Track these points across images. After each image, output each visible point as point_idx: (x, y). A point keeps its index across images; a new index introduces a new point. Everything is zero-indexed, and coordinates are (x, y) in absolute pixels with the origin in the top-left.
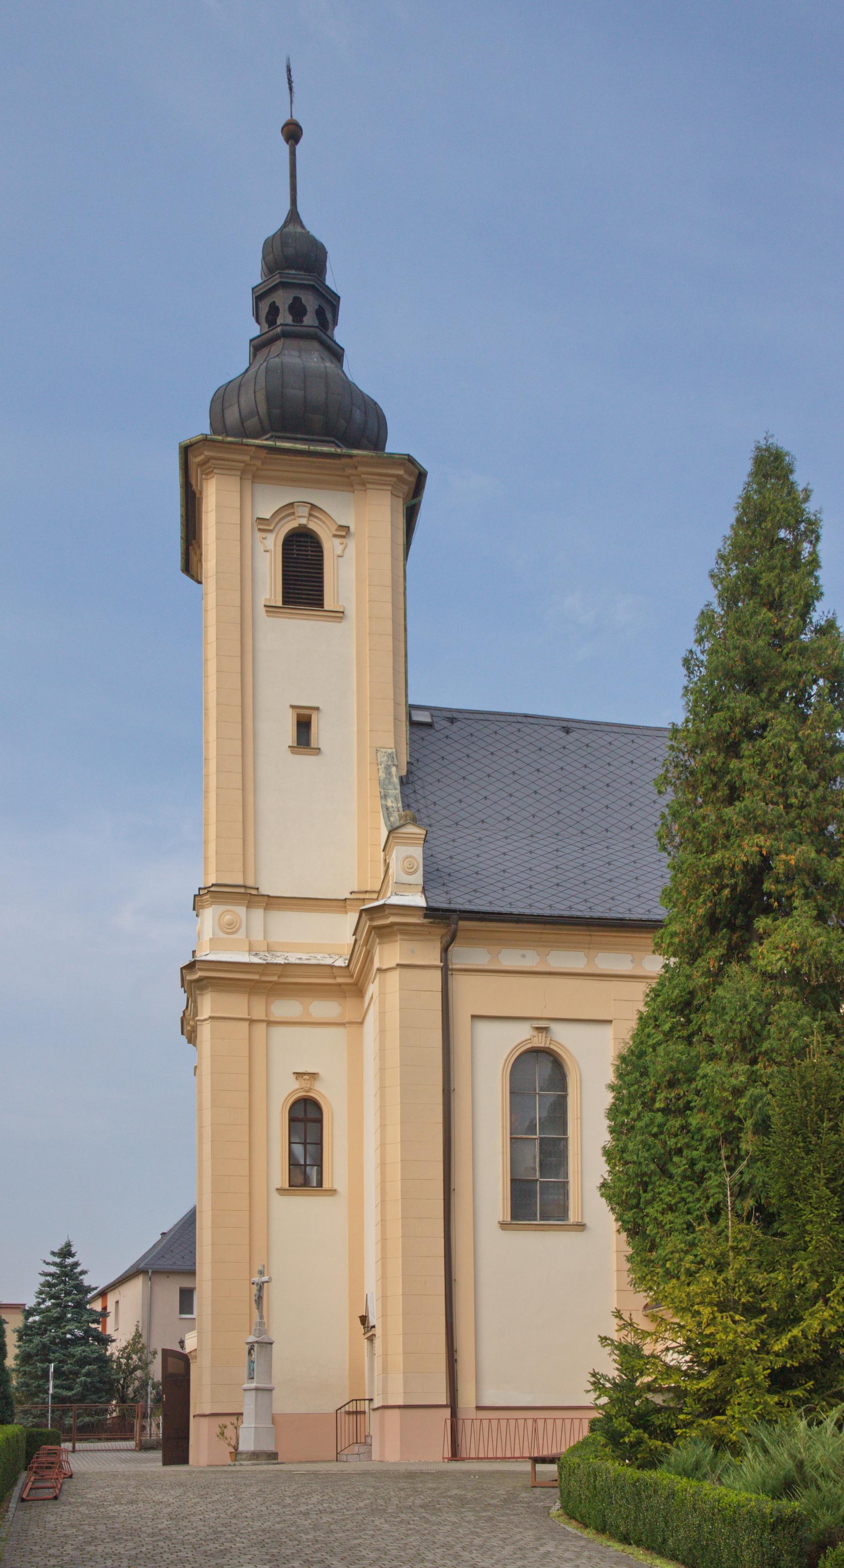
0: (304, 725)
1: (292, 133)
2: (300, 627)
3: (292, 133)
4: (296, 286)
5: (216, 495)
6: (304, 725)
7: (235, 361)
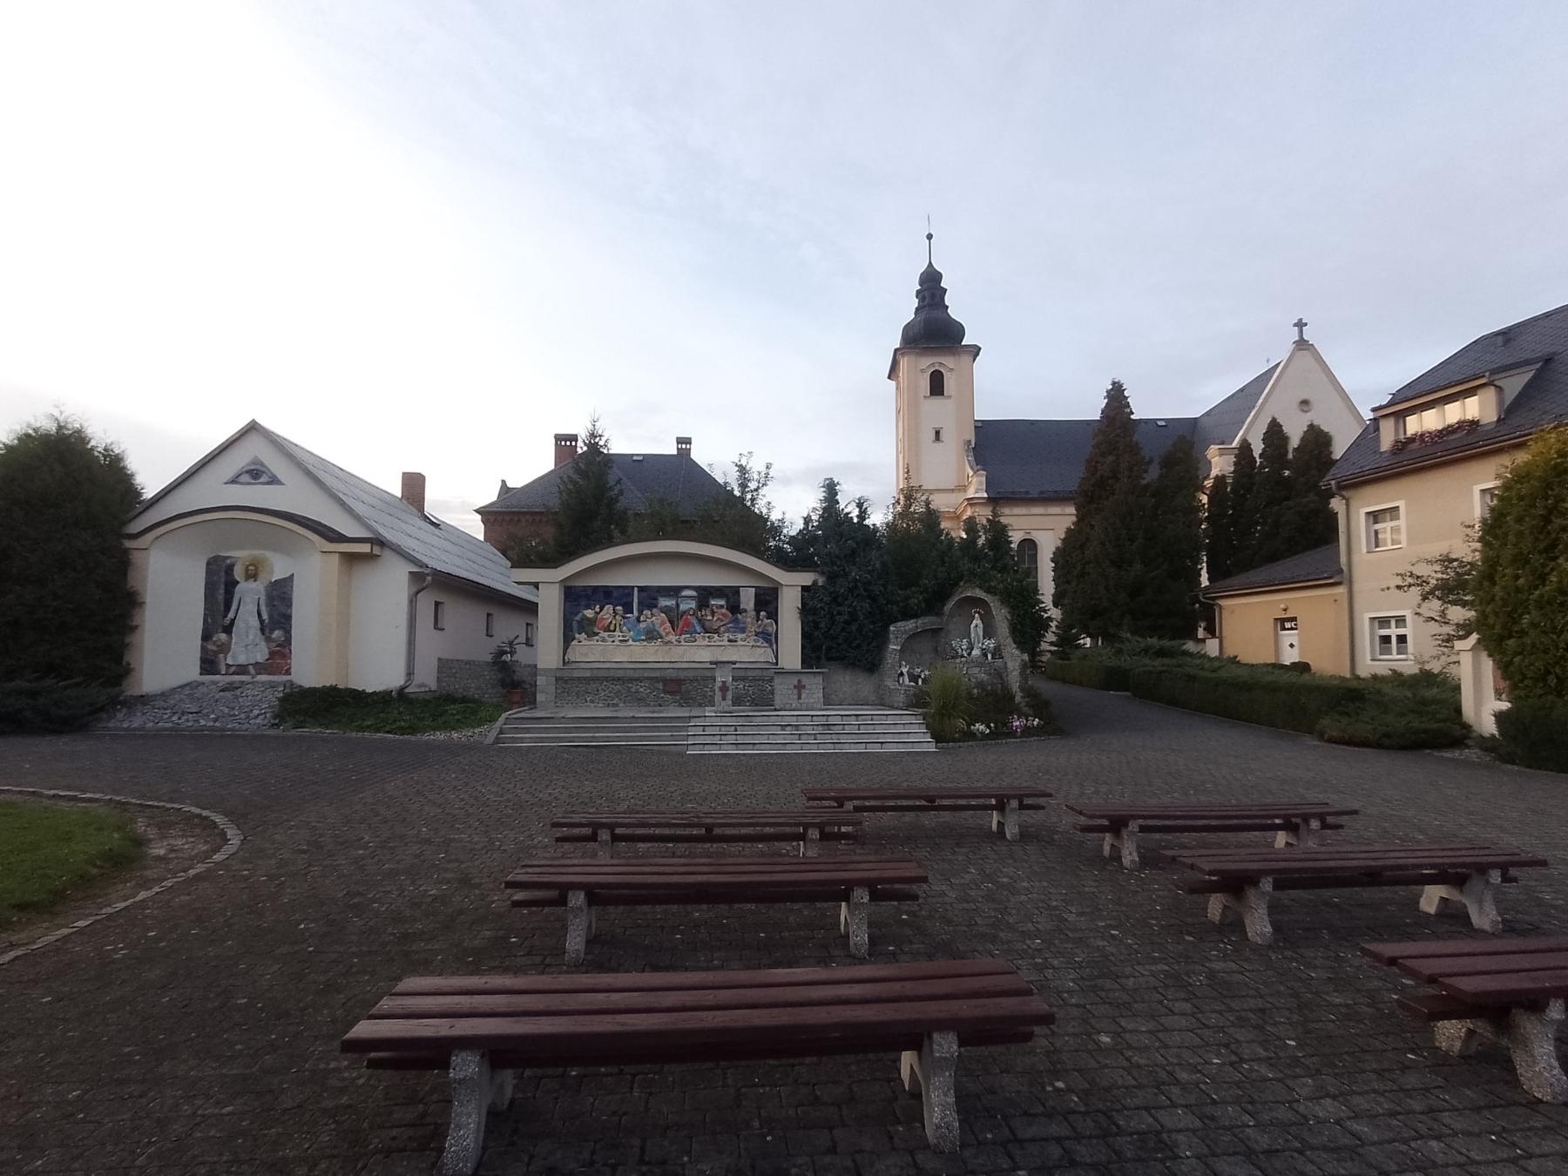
0: (937, 433)
1: (930, 237)
2: (937, 401)
3: (930, 237)
4: (931, 288)
5: (904, 363)
6: (937, 433)
7: (910, 316)
